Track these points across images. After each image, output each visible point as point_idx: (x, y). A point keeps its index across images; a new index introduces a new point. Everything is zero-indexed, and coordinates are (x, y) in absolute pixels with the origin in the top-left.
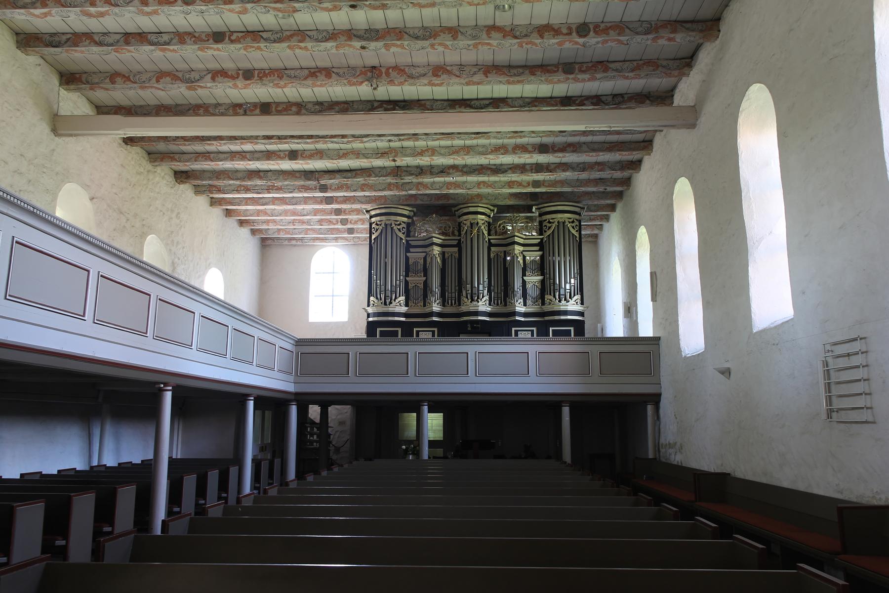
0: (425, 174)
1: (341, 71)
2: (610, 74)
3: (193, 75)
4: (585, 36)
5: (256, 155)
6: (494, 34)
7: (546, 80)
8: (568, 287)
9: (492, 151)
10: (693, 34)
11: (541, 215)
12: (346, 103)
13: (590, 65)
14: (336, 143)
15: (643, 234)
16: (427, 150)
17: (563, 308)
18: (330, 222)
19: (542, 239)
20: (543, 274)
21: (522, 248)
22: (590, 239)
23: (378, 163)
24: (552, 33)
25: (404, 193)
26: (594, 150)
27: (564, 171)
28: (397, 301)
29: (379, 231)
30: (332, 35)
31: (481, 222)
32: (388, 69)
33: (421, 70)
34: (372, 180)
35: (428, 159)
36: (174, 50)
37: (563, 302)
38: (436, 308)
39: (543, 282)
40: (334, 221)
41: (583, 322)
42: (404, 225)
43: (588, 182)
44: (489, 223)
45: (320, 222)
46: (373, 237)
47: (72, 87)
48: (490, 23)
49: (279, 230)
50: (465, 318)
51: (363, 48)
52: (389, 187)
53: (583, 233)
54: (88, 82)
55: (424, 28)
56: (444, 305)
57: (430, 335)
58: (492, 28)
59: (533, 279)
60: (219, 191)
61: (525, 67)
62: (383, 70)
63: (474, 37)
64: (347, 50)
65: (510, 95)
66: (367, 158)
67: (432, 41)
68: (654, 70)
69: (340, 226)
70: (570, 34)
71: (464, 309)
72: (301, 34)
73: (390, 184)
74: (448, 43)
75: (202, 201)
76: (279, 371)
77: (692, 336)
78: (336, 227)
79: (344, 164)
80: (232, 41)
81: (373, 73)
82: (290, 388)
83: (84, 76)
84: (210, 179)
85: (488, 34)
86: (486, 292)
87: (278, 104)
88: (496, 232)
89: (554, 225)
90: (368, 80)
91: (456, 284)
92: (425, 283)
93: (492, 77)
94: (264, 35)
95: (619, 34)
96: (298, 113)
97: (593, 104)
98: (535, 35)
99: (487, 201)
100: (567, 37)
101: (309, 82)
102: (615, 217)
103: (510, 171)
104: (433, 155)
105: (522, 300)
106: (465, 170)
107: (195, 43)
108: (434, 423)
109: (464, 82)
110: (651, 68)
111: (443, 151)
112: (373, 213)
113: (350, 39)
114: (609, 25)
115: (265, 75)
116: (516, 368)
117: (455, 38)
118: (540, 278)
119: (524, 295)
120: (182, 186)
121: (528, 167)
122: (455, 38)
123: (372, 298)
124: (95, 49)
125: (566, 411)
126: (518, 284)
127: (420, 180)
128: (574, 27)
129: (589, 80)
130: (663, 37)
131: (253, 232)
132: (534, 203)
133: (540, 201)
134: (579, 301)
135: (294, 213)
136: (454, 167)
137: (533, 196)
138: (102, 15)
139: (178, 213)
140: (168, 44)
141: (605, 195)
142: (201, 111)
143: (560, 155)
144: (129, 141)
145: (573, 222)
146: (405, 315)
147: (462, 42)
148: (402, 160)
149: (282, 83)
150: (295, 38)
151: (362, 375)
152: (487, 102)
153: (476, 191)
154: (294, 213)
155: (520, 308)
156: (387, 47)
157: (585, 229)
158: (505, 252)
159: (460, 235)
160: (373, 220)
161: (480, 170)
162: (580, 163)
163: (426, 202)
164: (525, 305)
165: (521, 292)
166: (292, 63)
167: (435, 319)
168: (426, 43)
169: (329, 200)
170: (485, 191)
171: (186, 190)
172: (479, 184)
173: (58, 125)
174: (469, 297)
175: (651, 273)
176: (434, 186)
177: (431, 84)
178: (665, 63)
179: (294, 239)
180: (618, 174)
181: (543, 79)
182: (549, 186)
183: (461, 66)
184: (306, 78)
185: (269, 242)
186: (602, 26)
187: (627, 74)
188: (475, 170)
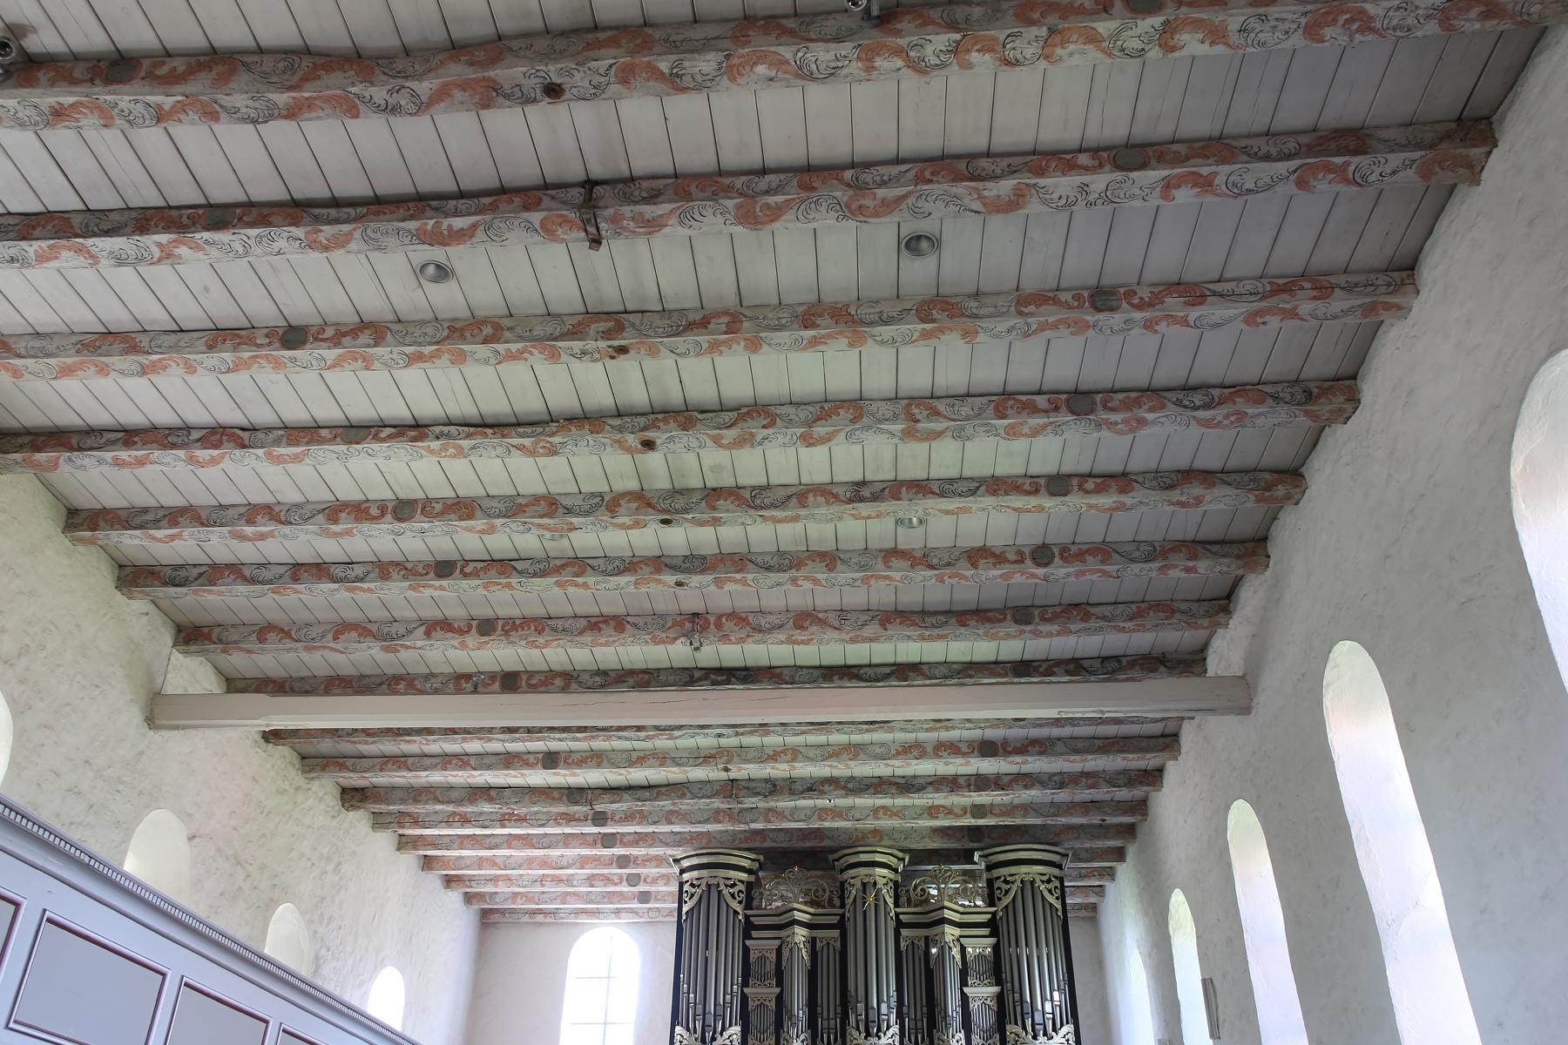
1: (641, 621)
4: (1046, 565)
5: (487, 760)
7: (986, 635)
8: (1048, 1008)
9: (898, 753)
10: (1226, 561)
11: (989, 868)
12: (646, 671)
14: (627, 739)
15: (1179, 904)
18: (608, 880)
19: (994, 914)
20: (999, 982)
21: (957, 932)
22: (1083, 913)
23: (698, 773)
26: (1077, 751)
27: (1026, 787)
28: (726, 1035)
29: (696, 898)
30: (629, 565)
31: (880, 882)
32: (720, 617)
34: (686, 804)
35: (784, 766)
36: (369, 590)
37: (1041, 1038)
39: (1000, 998)
40: (616, 879)
42: (741, 887)
43: (1071, 807)
44: (896, 883)
45: (591, 880)
46: (685, 909)
47: (193, 648)
48: (890, 545)
49: (515, 895)
51: (679, 584)
52: (716, 816)
53: (1068, 901)
60: (416, 822)
62: (712, 619)
69: (624, 888)
72: (579, 564)
73: (718, 811)
74: (820, 576)
75: (384, 841)
78: (618, 889)
79: (638, 775)
80: (465, 576)
81: (695, 623)
84: (403, 801)
86: (893, 1017)
87: (531, 674)
88: (909, 900)
89: (1014, 888)
93: (893, 630)
94: (519, 565)
95: (1102, 562)
97: (1068, 673)
98: (964, 563)
99: (891, 843)
101: (587, 638)
102: (1124, 870)
103: (930, 788)
106: (488, 330)
109: (847, 637)
112: (686, 863)
113: (658, 571)
114: (1084, 547)
115: (515, 627)
117: (831, 568)
120: (351, 814)
121: (961, 781)
122: (831, 568)
123: (678, 1029)
124: (243, 589)
128: (1027, 551)
130: (1175, 567)
131: (469, 898)
132: (975, 845)
133: (987, 841)
135: (545, 863)
136: (832, 781)
137: (975, 832)
139: (339, 864)
141: (1103, 830)
142: (401, 687)
143: (1018, 759)
144: (272, 736)
147: (843, 575)
148: (740, 769)
149: (541, 640)
152: (888, 670)
153: (871, 823)
154: (545, 863)
156: (719, 583)
157: (1072, 894)
158: (927, 938)
159: (843, 906)
160: (686, 876)
161: (878, 785)
162: (1055, 774)
165: (959, 1018)
169: (608, 841)
170: (886, 823)
171: (358, 820)
172: (876, 811)
173: (159, 709)
174: (862, 1028)
175: (1204, 981)
177: (791, 641)
178: (1184, 606)
179: (540, 911)
182: (1002, 814)
183: (842, 612)
184: (581, 633)
185: (495, 917)
186: (1074, 549)
188: (868, 787)
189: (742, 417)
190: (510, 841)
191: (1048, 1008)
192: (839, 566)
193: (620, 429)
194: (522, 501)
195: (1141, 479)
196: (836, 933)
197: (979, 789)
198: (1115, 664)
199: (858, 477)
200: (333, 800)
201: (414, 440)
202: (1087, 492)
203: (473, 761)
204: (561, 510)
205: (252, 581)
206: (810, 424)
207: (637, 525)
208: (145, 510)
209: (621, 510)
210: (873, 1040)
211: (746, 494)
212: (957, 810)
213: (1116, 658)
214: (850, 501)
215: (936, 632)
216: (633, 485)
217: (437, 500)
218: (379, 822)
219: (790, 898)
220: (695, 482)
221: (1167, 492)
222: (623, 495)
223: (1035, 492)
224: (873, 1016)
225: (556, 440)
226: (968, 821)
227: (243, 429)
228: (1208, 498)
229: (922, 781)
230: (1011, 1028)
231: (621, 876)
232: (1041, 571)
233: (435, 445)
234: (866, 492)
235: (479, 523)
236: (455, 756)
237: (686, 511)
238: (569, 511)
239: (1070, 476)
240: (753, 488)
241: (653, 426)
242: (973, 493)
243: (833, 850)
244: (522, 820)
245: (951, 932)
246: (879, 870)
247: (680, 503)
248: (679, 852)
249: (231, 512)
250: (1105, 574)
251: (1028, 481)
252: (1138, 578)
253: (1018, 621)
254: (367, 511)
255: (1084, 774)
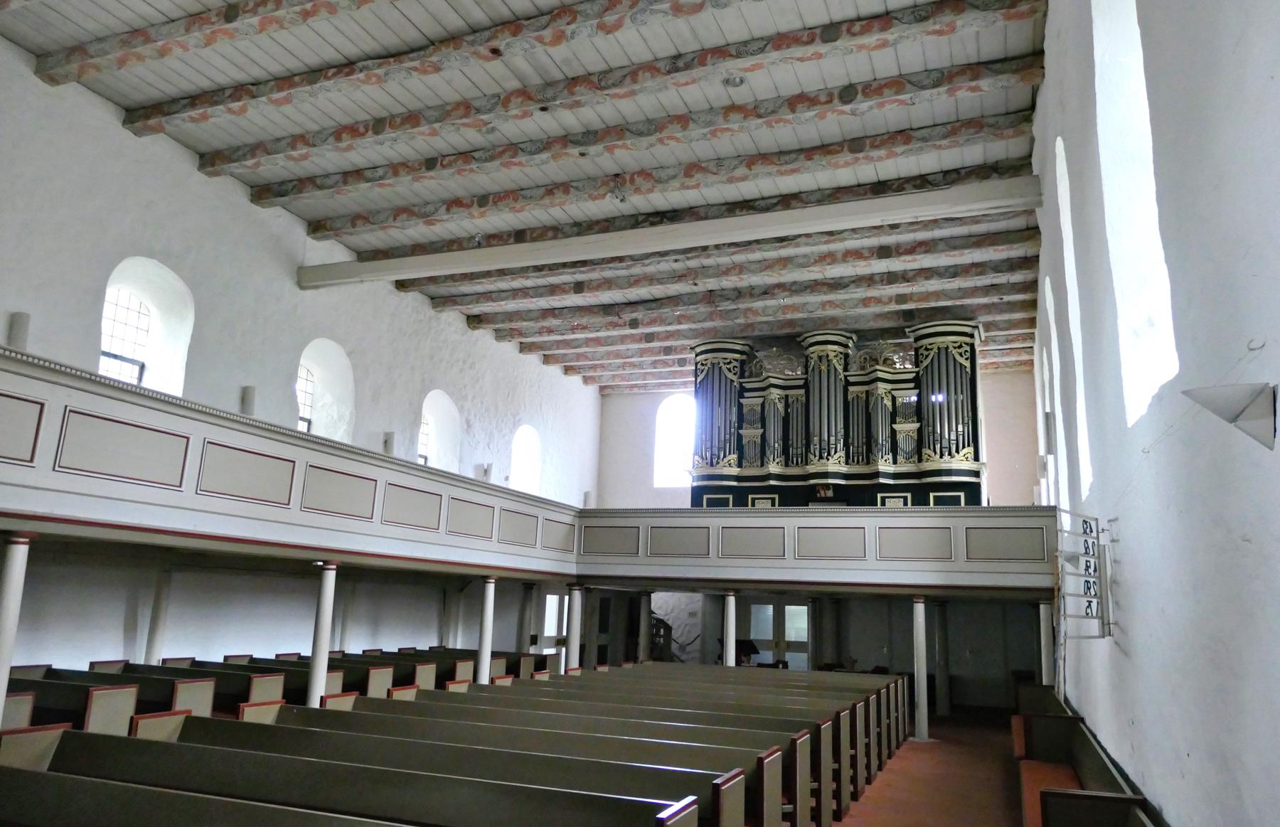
0: (744, 297)
1: (580, 185)
2: (915, 145)
3: (430, 208)
4: (850, 102)
6: (735, 116)
7: (829, 164)
9: (816, 262)
10: (1005, 76)
12: (607, 220)
13: (886, 137)
16: (734, 268)
17: (944, 466)
18: (665, 363)
19: (918, 373)
20: (919, 420)
21: (889, 386)
24: (807, 104)
25: (730, 323)
26: (955, 248)
28: (962, 453)
30: (546, 144)
31: (832, 355)
32: (633, 175)
33: (671, 172)
35: (734, 278)
36: (390, 185)
37: (946, 457)
38: (774, 468)
39: (920, 431)
41: (978, 486)
43: (974, 291)
47: (318, 235)
48: (727, 102)
50: (812, 482)
51: (582, 155)
52: (711, 317)
54: (331, 229)
55: (649, 121)
56: (787, 465)
57: (768, 504)
58: (732, 108)
59: (906, 428)
61: (801, 150)
62: (628, 177)
63: (709, 124)
64: (563, 162)
65: (804, 188)
66: (661, 283)
67: (658, 135)
68: (976, 133)
70: (830, 101)
71: (811, 469)
72: (513, 148)
74: (679, 135)
75: (509, 348)
76: (544, 547)
77: (1065, 504)
80: (443, 166)
81: (617, 181)
82: (572, 569)
83: (329, 223)
85: (726, 115)
87: (533, 230)
89: (932, 353)
90: (612, 192)
91: (797, 437)
92: (763, 436)
93: (759, 168)
94: (476, 155)
95: (897, 93)
96: (555, 238)
97: (916, 187)
98: (785, 109)
100: (827, 106)
101: (547, 201)
104: (741, 272)
105: (890, 456)
107: (408, 173)
108: (798, 621)
109: (724, 179)
110: (972, 130)
111: (753, 267)
112: (698, 350)
113: (565, 146)
114: (883, 82)
115: (500, 199)
116: (878, 548)
117: (684, 128)
118: (918, 425)
119: (894, 449)
120: (476, 332)
121: (877, 278)
122: (684, 128)
124: (319, 193)
125: (920, 609)
126: (882, 435)
127: (749, 305)
128: (836, 93)
129: (888, 157)
130: (960, 88)
131: (586, 380)
133: (917, 320)
134: (971, 456)
135: (618, 355)
136: (781, 286)
137: (909, 315)
138: (305, 157)
139: (473, 364)
140: (381, 178)
142: (455, 247)
143: (908, 258)
144: (401, 285)
145: (960, 347)
146: (846, 476)
147: (695, 131)
149: (518, 206)
150: (508, 154)
151: (654, 554)
152: (775, 201)
153: (820, 313)
155: (885, 465)
156: (610, 149)
160: (699, 358)
161: (814, 286)
163: (766, 331)
164: (895, 462)
165: (888, 445)
166: (525, 182)
167: (772, 482)
168: (653, 139)
169: (649, 338)
170: (831, 312)
171: (484, 336)
172: (824, 305)
173: (306, 277)
176: (768, 312)
177: (684, 187)
178: (991, 121)
179: (635, 386)
180: (1017, 277)
181: (824, 163)
182: (919, 300)
183: (719, 161)
184: (542, 198)
185: (607, 391)
186: (875, 85)
187: (938, 143)
188: (806, 288)
189: (554, 19)
190: (588, 342)
191: (953, 437)
192: (692, 125)
193: (472, 43)
194: (448, 108)
195: (900, 16)
196: (802, 391)
197: (890, 282)
198: (954, 176)
199: (673, 52)
200: (461, 323)
201: (348, 74)
202: (854, 35)
203: (531, 292)
204: (473, 111)
205: (321, 187)
206: (600, 15)
207: (526, 114)
208: (238, 148)
209: (512, 105)
210: (824, 461)
211: (595, 79)
212: (885, 300)
213: (956, 171)
214: (669, 72)
215: (790, 167)
216: (514, 84)
217: (398, 115)
218: (500, 335)
219: (779, 371)
220: (559, 76)
221: (924, 24)
222: (512, 94)
223: (811, 41)
224: (825, 445)
225: (434, 59)
226: (894, 307)
227: (253, 84)
228: (959, 23)
229: (846, 281)
230: (926, 451)
231: (673, 360)
232: (847, 108)
233: (361, 76)
234: (681, 64)
235: (424, 128)
236: (520, 290)
237: (554, 99)
238: (478, 111)
239: (840, 23)
240: (601, 73)
241: (494, 37)
242: (762, 50)
243: (799, 335)
244: (584, 328)
245: (882, 387)
246: (830, 347)
247: (550, 93)
248: (692, 343)
249: (283, 143)
250: (902, 102)
251: (806, 33)
252: (935, 105)
253: (852, 151)
254: (357, 130)
255: (974, 265)
